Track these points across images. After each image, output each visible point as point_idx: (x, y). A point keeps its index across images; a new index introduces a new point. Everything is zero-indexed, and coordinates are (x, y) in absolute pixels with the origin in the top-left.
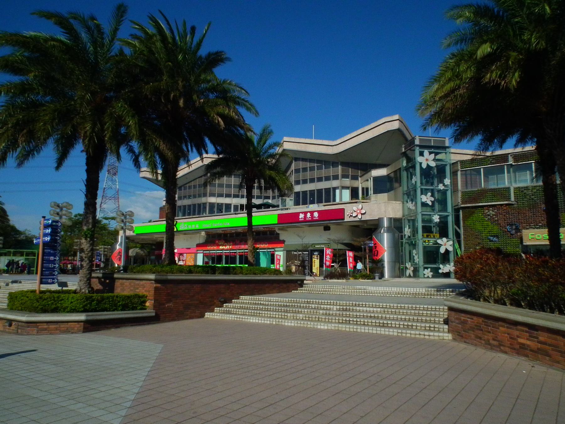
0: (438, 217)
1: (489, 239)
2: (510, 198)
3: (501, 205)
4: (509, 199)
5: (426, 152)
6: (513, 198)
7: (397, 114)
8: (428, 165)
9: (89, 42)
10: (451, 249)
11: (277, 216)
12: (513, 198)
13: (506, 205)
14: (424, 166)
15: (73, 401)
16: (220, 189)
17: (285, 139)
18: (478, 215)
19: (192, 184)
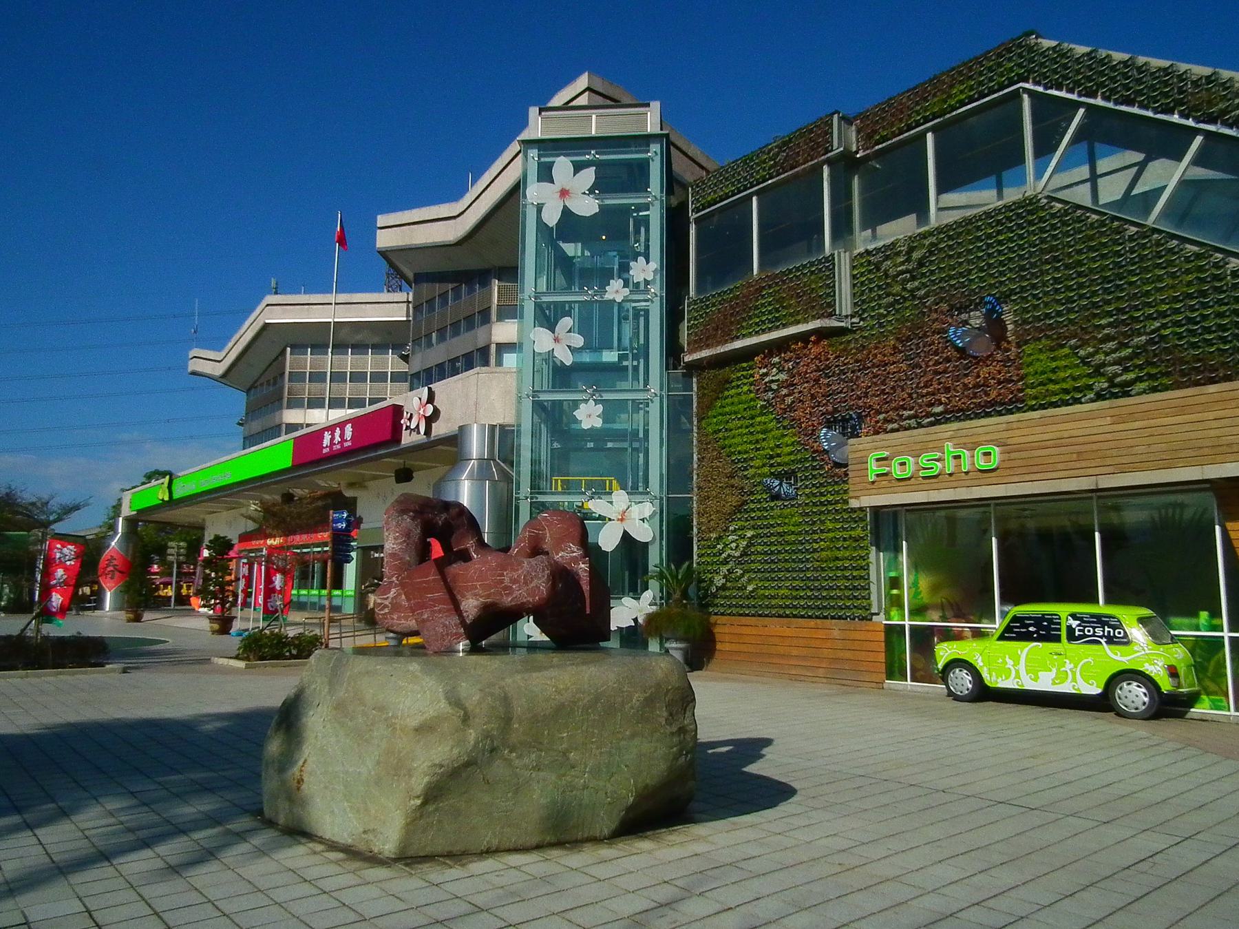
0: (600, 408)
1: (769, 489)
2: (831, 305)
3: (804, 337)
4: (828, 310)
5: (562, 165)
6: (845, 301)
7: (580, 73)
8: (566, 212)
9: (602, 200)
10: (644, 533)
11: (291, 444)
12: (845, 301)
13: (821, 334)
14: (552, 217)
15: (995, 680)
16: (317, 386)
17: (382, 220)
18: (741, 392)
19: (262, 380)
